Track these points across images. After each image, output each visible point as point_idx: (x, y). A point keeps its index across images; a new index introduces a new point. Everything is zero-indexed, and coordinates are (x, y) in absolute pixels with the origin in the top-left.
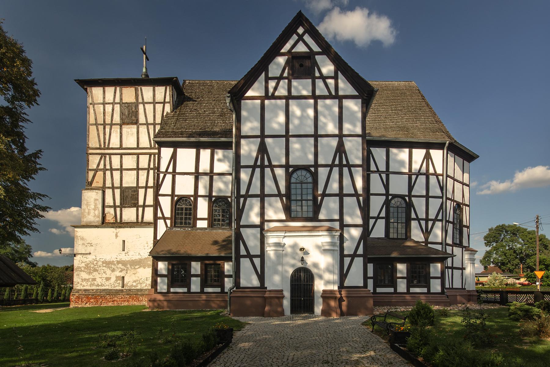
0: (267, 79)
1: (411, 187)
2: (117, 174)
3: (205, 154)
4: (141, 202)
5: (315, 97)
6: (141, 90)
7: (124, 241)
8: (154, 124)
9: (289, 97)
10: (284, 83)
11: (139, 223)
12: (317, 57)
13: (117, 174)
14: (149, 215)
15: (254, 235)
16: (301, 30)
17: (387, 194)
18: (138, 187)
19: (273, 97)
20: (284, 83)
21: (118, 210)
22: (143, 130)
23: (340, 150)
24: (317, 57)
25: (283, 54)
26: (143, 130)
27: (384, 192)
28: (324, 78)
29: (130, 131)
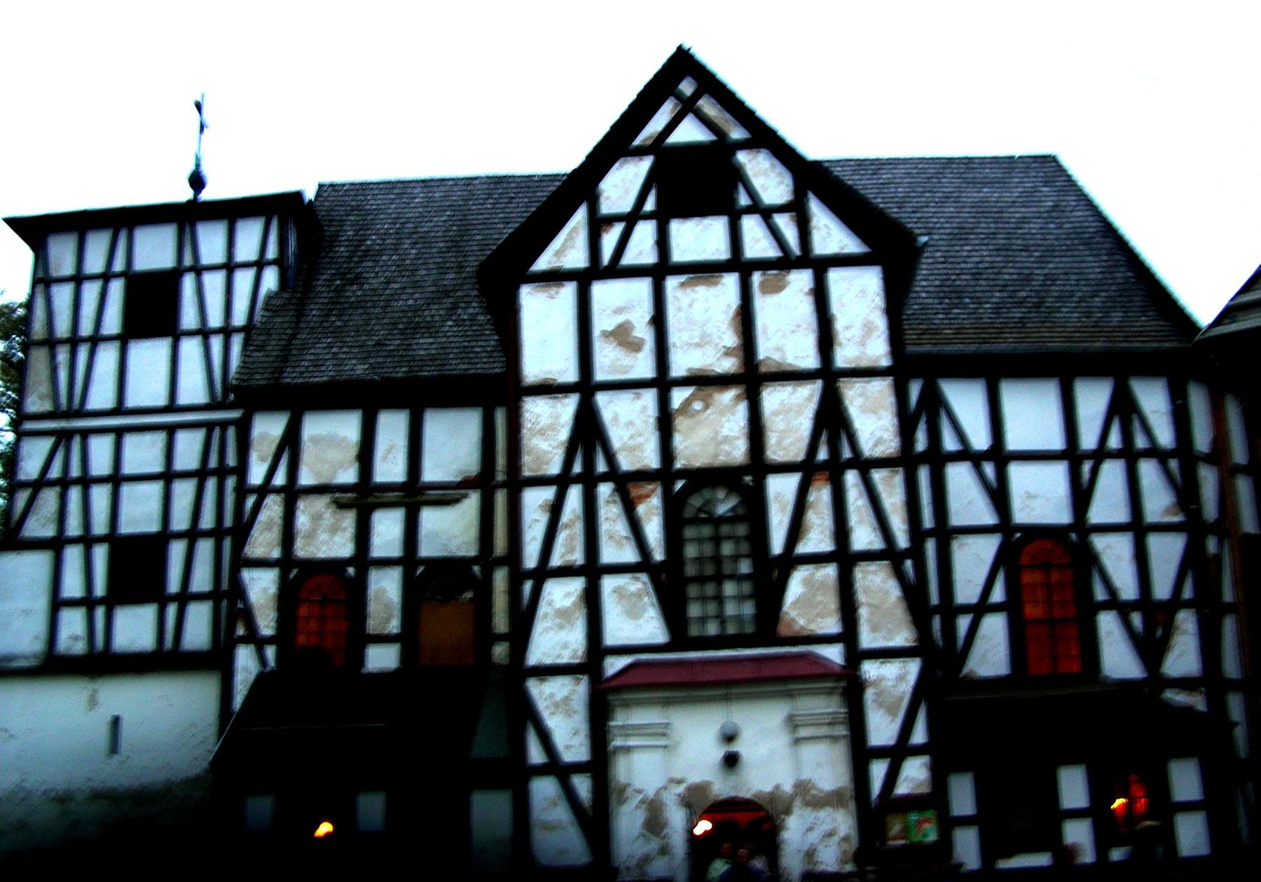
0: (597, 225)
1: (1081, 495)
2: (100, 495)
3: (392, 428)
4: (174, 585)
5: (738, 264)
8: (227, 331)
9: (661, 270)
10: (645, 233)
11: (165, 660)
12: (742, 157)
13: (100, 495)
14: (198, 628)
15: (563, 705)
16: (687, 87)
18: (164, 537)
19: (616, 271)
20: (645, 233)
21: (100, 612)
22: (191, 349)
23: (832, 419)
24: (742, 157)
25: (640, 152)
26: (191, 349)
28: (767, 213)
29: (149, 356)
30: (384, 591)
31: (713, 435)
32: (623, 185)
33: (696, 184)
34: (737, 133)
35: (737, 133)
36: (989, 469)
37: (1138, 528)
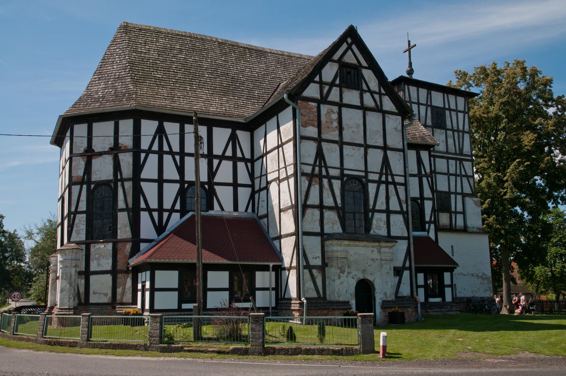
4: (453, 209)
6: (408, 89)
7: (452, 246)
17: (182, 181)
27: (177, 177)
28: (372, 93)
30: (517, 211)
31: (354, 161)
32: (329, 72)
33: (350, 77)
34: (364, 63)
35: (364, 63)
36: (249, 165)
37: (161, 181)
